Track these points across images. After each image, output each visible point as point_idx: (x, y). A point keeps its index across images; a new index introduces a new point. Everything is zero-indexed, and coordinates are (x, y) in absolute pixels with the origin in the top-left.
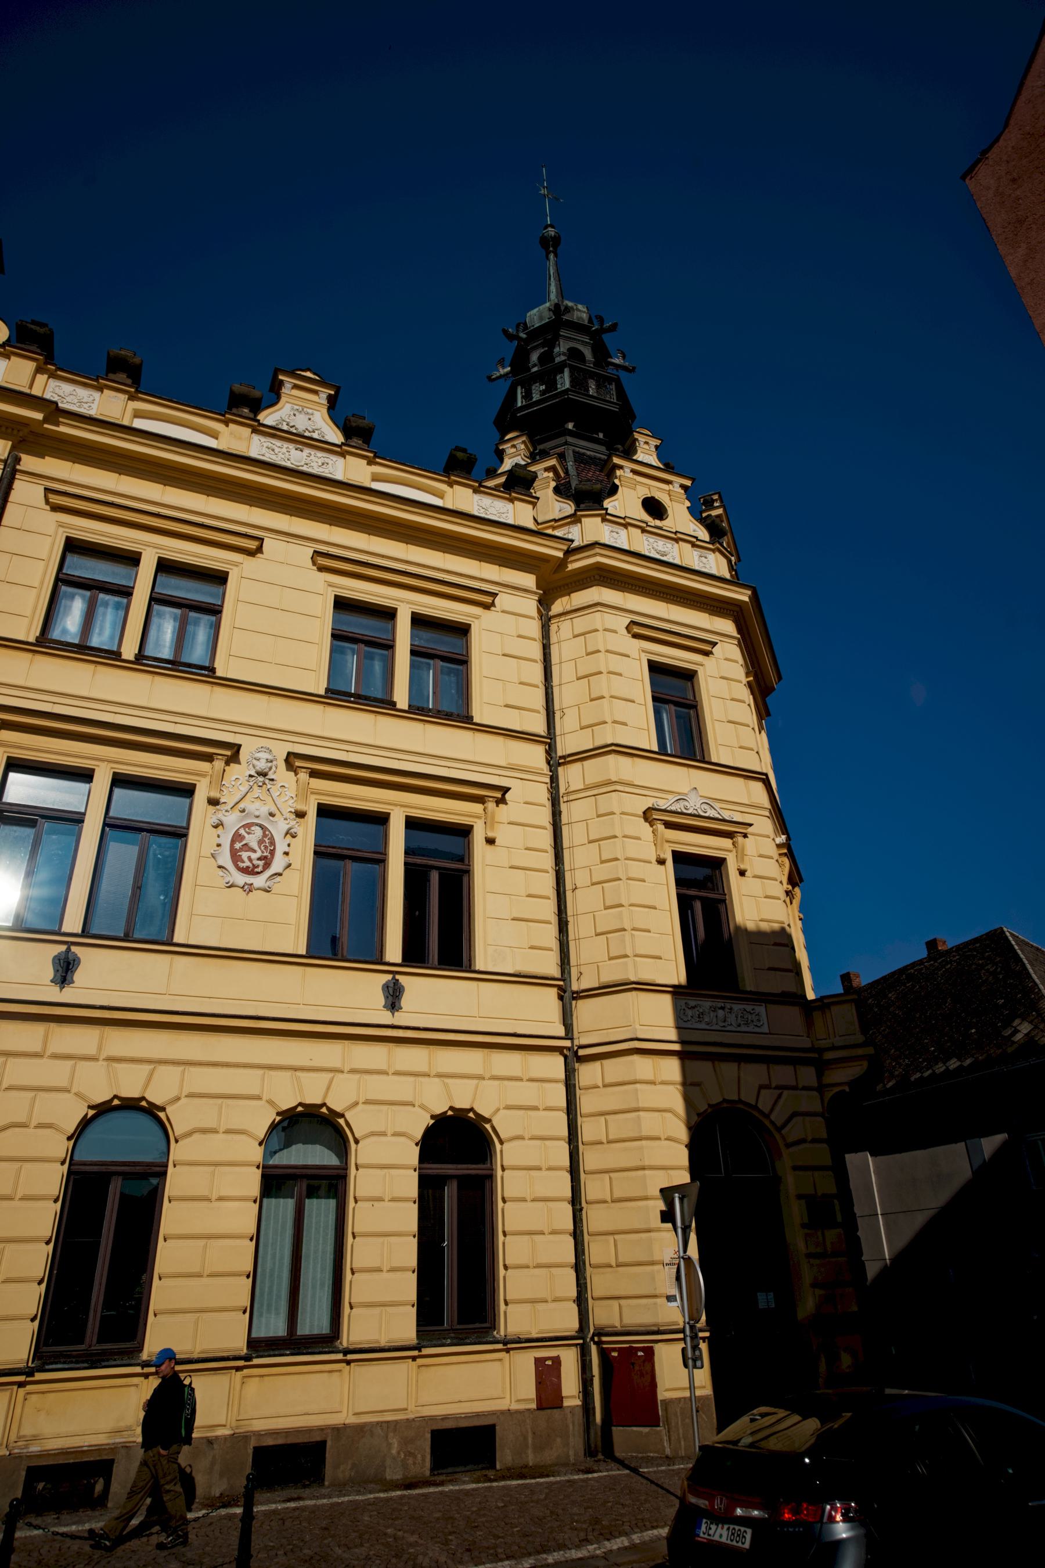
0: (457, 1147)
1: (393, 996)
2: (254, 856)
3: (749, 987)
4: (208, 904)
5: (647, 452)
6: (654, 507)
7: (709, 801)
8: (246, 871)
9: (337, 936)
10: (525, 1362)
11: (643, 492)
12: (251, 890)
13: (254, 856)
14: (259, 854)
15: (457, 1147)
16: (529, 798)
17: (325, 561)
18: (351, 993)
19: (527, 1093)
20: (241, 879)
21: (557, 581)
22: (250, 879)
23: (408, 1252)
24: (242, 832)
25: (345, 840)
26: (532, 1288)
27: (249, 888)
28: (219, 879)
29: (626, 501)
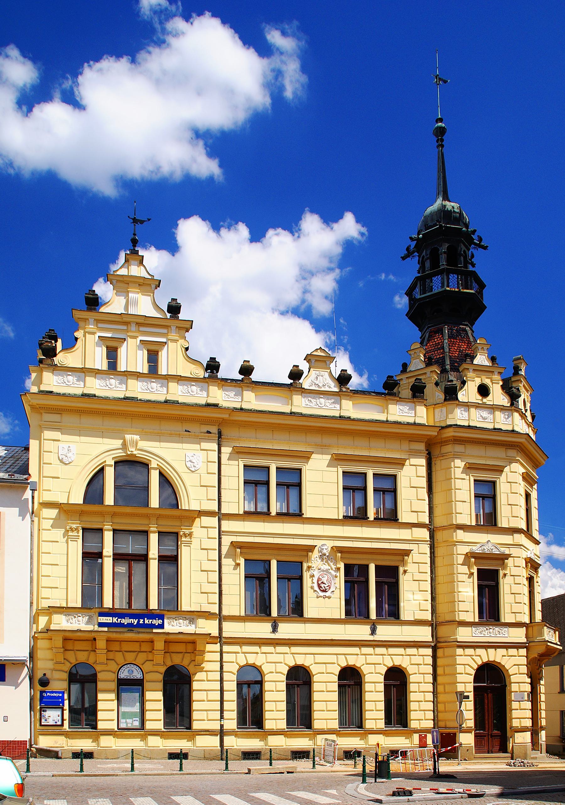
0: (396, 680)
1: (373, 632)
2: (325, 586)
3: (504, 525)
4: (312, 605)
5: (481, 359)
6: (483, 391)
7: (496, 546)
8: (323, 591)
9: (355, 609)
10: (416, 737)
11: (478, 381)
12: (325, 597)
13: (325, 586)
14: (327, 585)
15: (396, 680)
16: (420, 556)
17: (338, 459)
18: (360, 631)
19: (419, 660)
20: (322, 594)
21: (434, 446)
22: (324, 594)
23: (382, 706)
24: (320, 577)
25: (355, 577)
26: (420, 713)
27: (325, 597)
28: (315, 595)
29: (469, 393)
